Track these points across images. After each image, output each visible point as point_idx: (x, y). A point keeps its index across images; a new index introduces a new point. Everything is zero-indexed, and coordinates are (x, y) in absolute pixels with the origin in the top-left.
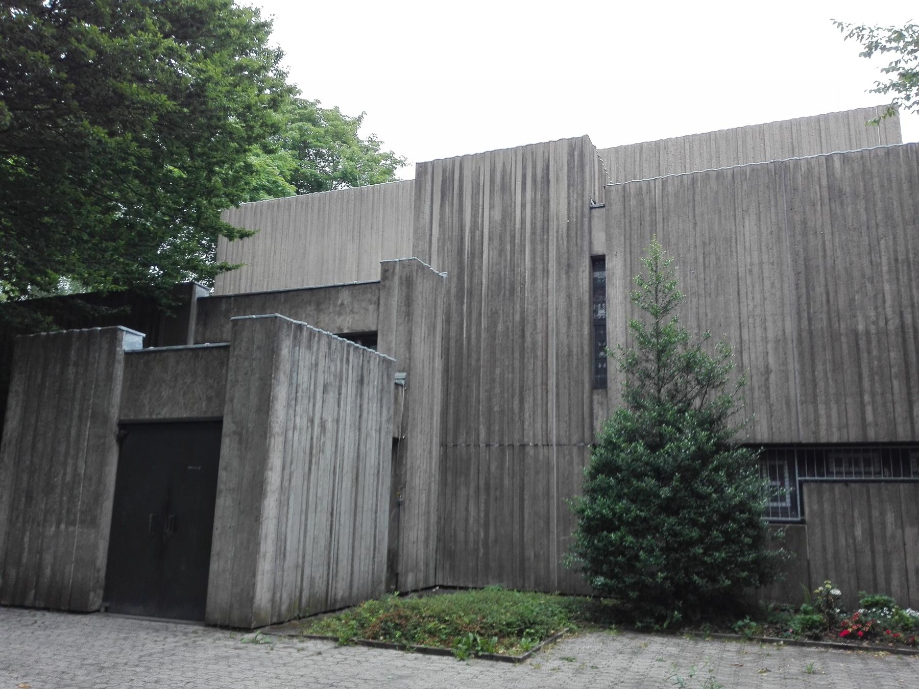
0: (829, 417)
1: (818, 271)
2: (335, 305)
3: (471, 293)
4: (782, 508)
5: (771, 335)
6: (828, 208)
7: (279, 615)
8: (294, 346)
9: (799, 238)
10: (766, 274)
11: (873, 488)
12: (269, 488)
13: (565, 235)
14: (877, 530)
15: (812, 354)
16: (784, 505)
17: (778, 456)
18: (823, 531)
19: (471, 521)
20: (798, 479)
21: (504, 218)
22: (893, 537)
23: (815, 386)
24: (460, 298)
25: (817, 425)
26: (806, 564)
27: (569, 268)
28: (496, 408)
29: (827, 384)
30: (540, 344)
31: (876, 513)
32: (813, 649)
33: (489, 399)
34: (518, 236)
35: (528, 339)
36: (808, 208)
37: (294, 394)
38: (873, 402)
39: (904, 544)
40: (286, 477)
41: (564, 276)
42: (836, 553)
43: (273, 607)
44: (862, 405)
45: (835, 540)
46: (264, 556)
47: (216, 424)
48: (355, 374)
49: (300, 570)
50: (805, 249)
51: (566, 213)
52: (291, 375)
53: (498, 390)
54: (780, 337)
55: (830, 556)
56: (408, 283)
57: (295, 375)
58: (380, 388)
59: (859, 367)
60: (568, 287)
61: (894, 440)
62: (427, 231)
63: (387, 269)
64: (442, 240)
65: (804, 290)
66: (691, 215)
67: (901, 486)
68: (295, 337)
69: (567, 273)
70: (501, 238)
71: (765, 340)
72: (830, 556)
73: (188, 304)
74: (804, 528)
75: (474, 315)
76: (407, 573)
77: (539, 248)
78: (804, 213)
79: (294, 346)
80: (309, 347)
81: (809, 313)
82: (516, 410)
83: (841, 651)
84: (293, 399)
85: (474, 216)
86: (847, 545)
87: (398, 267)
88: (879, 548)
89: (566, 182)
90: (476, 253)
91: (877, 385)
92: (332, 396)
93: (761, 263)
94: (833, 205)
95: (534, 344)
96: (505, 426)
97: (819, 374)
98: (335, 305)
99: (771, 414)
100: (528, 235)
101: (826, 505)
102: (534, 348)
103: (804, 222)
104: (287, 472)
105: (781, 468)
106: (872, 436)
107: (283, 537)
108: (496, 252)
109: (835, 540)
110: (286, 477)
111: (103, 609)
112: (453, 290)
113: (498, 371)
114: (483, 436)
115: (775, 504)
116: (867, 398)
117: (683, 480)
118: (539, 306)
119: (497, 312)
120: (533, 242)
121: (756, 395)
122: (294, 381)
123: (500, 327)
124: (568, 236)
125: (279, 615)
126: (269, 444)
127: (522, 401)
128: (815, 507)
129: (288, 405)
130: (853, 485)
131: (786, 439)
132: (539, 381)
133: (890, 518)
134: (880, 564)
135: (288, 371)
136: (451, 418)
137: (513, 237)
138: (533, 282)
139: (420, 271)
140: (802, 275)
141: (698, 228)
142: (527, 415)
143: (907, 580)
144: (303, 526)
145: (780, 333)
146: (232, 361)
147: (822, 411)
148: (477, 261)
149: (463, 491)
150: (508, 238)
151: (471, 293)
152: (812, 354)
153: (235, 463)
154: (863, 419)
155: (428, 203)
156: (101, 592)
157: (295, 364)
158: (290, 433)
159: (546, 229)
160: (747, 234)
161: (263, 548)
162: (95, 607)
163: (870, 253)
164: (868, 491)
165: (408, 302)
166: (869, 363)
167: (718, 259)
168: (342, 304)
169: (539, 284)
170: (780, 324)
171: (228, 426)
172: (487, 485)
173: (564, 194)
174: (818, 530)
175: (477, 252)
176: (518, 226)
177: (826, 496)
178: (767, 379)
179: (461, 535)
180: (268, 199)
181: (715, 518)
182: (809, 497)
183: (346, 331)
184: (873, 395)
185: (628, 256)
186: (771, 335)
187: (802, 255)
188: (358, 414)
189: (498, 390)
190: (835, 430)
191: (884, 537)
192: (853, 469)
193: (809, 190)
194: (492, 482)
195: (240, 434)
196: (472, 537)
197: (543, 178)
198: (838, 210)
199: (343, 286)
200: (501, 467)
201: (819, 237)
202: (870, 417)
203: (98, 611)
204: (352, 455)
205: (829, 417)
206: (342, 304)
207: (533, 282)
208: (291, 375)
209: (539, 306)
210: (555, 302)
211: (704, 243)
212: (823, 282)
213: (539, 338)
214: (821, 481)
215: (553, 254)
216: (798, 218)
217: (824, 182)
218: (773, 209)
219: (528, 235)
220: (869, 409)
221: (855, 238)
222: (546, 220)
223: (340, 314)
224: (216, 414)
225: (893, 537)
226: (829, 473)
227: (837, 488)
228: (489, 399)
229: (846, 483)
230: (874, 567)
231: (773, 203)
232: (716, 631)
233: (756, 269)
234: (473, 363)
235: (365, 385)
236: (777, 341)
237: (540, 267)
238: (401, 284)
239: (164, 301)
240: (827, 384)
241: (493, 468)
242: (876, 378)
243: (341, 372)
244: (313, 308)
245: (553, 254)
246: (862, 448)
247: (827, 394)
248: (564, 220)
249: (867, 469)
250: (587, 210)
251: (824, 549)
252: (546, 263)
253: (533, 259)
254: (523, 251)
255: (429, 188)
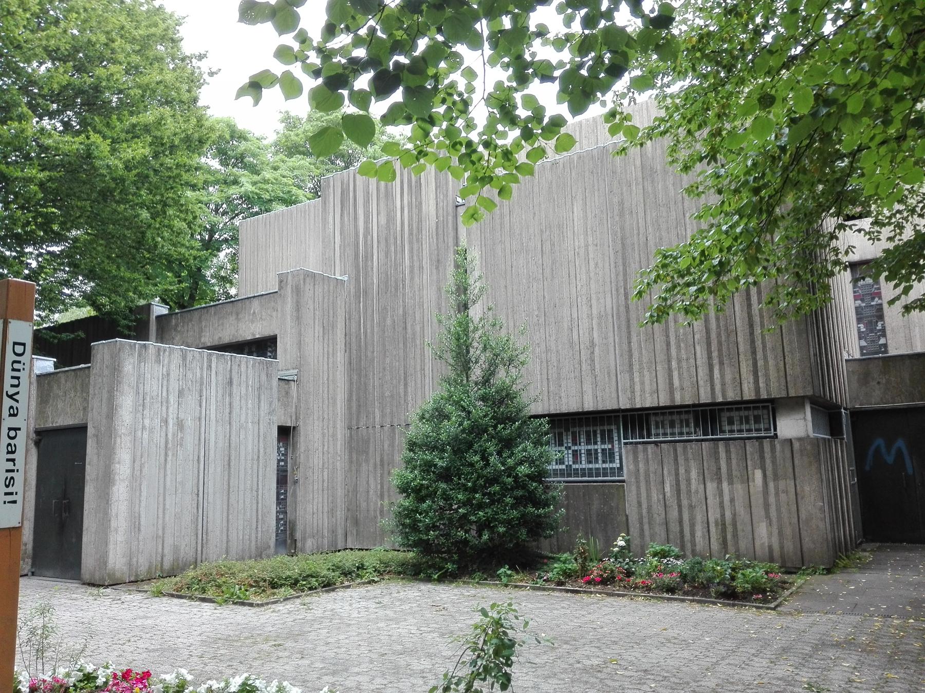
0: (642, 383)
1: (633, 249)
2: (249, 314)
3: (366, 292)
4: (611, 469)
5: (595, 312)
6: (641, 187)
7: (137, 575)
8: (140, 362)
9: (617, 218)
10: (591, 256)
11: (679, 446)
12: (117, 477)
13: (434, 233)
14: (683, 487)
15: (628, 327)
16: (597, 466)
17: (566, 424)
18: (638, 487)
19: (371, 492)
20: (623, 441)
21: (388, 221)
22: (697, 492)
23: (631, 356)
24: (357, 297)
25: (633, 392)
26: (624, 519)
27: (438, 263)
28: (387, 394)
29: (641, 353)
30: (418, 333)
31: (682, 471)
32: (557, 594)
33: (382, 386)
34: (399, 238)
35: (409, 330)
36: (625, 189)
37: (141, 402)
38: (680, 368)
39: (706, 499)
40: (137, 468)
41: (435, 271)
42: (650, 508)
43: (130, 569)
44: (670, 370)
45: (649, 497)
46: (116, 530)
47: (82, 429)
48: (220, 378)
49: (160, 541)
50: (622, 229)
51: (434, 213)
52: (138, 386)
53: (388, 378)
54: (603, 313)
55: (644, 511)
56: (297, 291)
57: (141, 386)
58: (257, 385)
59: (668, 336)
60: (438, 281)
61: (697, 402)
62: (332, 239)
63: (282, 281)
64: (343, 247)
65: (621, 268)
66: (531, 206)
67: (639, 446)
68: (140, 355)
69: (437, 268)
70: (386, 241)
71: (590, 316)
72: (644, 511)
73: (147, 322)
74: (623, 486)
75: (369, 312)
76: (304, 539)
77: (415, 246)
78: (622, 194)
79: (140, 362)
80: (158, 361)
81: (625, 289)
82: (402, 394)
83: (569, 595)
84: (141, 405)
85: (367, 222)
86: (659, 500)
87: (290, 278)
88: (685, 502)
89: (434, 184)
90: (368, 257)
91: (683, 352)
92: (191, 400)
93: (587, 246)
94: (646, 184)
95: (414, 334)
96: (395, 409)
97: (634, 345)
98: (249, 314)
99: (595, 384)
100: (406, 236)
101: (641, 465)
102: (414, 339)
103: (621, 203)
104: (137, 463)
105: (610, 431)
106: (678, 401)
107: (137, 515)
108: (383, 254)
109: (649, 497)
110: (137, 468)
111: (30, 574)
112: (353, 290)
113: (388, 360)
114: (377, 419)
115: (590, 466)
116: (674, 364)
117: (455, 452)
118: (417, 300)
119: (385, 308)
120: (411, 242)
121: (584, 366)
122: (141, 391)
123: (389, 322)
124: (437, 234)
125: (137, 575)
126: (115, 443)
127: (406, 385)
128: (632, 467)
129: (136, 411)
130: (663, 445)
131: (609, 406)
132: (418, 367)
133: (694, 474)
134: (686, 517)
135: (134, 383)
136: (354, 405)
137: (396, 239)
138: (412, 279)
139: (308, 280)
140: (620, 254)
141: (536, 218)
142: (410, 399)
143: (709, 531)
144: (161, 506)
145: (603, 309)
146: (92, 378)
147: (637, 380)
148: (369, 263)
149: (364, 467)
150: (392, 240)
151: (366, 292)
152: (628, 327)
153: (95, 457)
154: (671, 384)
155: (331, 214)
156: (30, 561)
157: (140, 378)
158: (139, 433)
159: (420, 230)
160: (576, 219)
161: (113, 524)
162: (25, 572)
163: (677, 228)
164: (675, 450)
165: (298, 307)
166: (676, 331)
167: (553, 245)
168: (254, 313)
169: (416, 279)
170: (602, 301)
171: (91, 431)
172: (382, 460)
173: (432, 196)
174: (634, 488)
175: (369, 256)
176: (399, 228)
177: (641, 456)
178: (593, 353)
179: (364, 505)
180: (279, 208)
181: (481, 482)
182: (627, 458)
183: (209, 344)
184: (679, 361)
185: (483, 248)
186: (595, 312)
187: (619, 235)
188: (228, 411)
189: (388, 378)
190: (647, 395)
191: (689, 492)
192: (669, 431)
193: (626, 171)
194: (385, 458)
195: (97, 436)
196: (372, 508)
197: (416, 182)
198: (650, 188)
199: (254, 297)
200: (392, 445)
201: (634, 216)
202: (676, 383)
203: (26, 575)
204: (220, 445)
205: (642, 383)
206: (254, 313)
207: (412, 279)
208: (138, 386)
209: (417, 300)
210: (429, 295)
211: (541, 230)
212: (637, 259)
213: (418, 328)
214: (637, 443)
215: (426, 252)
216: (616, 200)
217: (638, 163)
218: (596, 194)
219: (406, 236)
220: (675, 374)
221: (664, 214)
222: (420, 221)
223: (252, 322)
224: (84, 422)
225: (697, 492)
226: (722, 432)
227: (650, 448)
228: (382, 386)
229: (655, 443)
230: (681, 522)
231: (596, 188)
232: (486, 579)
233: (582, 251)
234: (369, 354)
235: (234, 387)
236: (600, 317)
237: (416, 264)
238: (292, 291)
239: (124, 322)
240: (641, 353)
241: (386, 446)
242: (682, 345)
243: (202, 378)
244: (234, 317)
245: (426, 252)
246: (761, 405)
247: (641, 363)
248: (433, 220)
249: (757, 426)
250: (450, 209)
251: (640, 504)
252: (421, 261)
253: (411, 257)
254: (403, 251)
255: (332, 200)
